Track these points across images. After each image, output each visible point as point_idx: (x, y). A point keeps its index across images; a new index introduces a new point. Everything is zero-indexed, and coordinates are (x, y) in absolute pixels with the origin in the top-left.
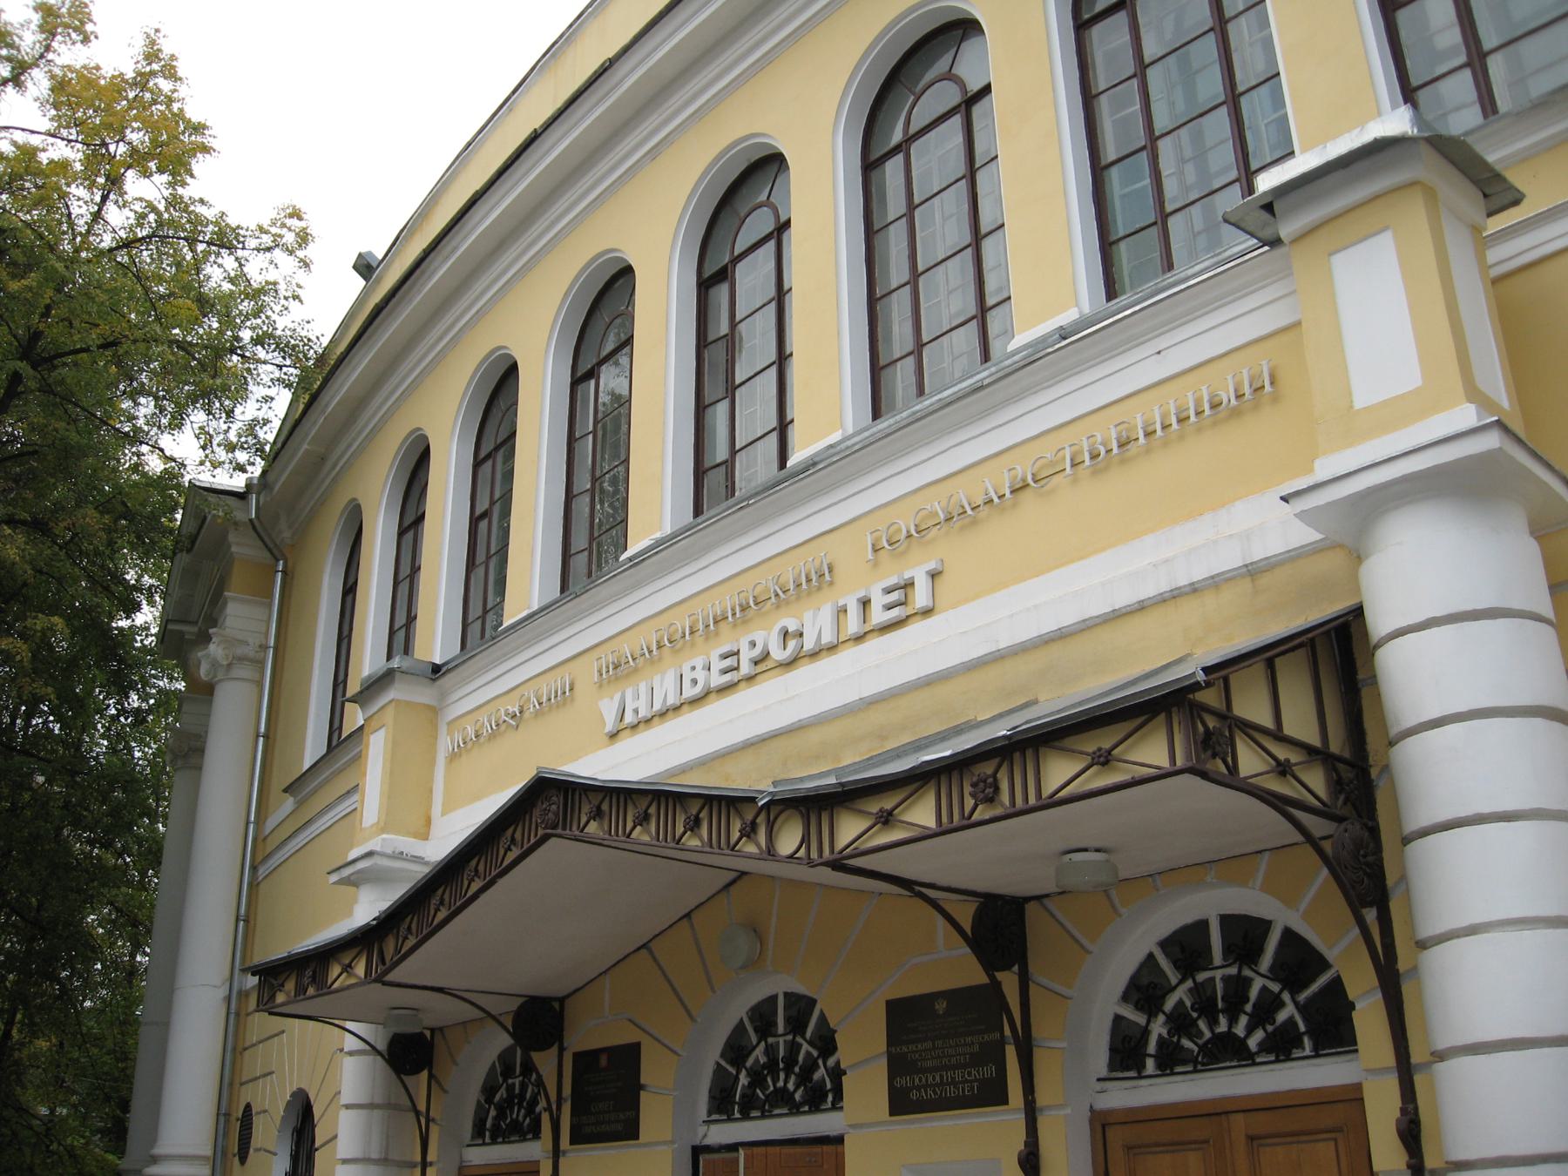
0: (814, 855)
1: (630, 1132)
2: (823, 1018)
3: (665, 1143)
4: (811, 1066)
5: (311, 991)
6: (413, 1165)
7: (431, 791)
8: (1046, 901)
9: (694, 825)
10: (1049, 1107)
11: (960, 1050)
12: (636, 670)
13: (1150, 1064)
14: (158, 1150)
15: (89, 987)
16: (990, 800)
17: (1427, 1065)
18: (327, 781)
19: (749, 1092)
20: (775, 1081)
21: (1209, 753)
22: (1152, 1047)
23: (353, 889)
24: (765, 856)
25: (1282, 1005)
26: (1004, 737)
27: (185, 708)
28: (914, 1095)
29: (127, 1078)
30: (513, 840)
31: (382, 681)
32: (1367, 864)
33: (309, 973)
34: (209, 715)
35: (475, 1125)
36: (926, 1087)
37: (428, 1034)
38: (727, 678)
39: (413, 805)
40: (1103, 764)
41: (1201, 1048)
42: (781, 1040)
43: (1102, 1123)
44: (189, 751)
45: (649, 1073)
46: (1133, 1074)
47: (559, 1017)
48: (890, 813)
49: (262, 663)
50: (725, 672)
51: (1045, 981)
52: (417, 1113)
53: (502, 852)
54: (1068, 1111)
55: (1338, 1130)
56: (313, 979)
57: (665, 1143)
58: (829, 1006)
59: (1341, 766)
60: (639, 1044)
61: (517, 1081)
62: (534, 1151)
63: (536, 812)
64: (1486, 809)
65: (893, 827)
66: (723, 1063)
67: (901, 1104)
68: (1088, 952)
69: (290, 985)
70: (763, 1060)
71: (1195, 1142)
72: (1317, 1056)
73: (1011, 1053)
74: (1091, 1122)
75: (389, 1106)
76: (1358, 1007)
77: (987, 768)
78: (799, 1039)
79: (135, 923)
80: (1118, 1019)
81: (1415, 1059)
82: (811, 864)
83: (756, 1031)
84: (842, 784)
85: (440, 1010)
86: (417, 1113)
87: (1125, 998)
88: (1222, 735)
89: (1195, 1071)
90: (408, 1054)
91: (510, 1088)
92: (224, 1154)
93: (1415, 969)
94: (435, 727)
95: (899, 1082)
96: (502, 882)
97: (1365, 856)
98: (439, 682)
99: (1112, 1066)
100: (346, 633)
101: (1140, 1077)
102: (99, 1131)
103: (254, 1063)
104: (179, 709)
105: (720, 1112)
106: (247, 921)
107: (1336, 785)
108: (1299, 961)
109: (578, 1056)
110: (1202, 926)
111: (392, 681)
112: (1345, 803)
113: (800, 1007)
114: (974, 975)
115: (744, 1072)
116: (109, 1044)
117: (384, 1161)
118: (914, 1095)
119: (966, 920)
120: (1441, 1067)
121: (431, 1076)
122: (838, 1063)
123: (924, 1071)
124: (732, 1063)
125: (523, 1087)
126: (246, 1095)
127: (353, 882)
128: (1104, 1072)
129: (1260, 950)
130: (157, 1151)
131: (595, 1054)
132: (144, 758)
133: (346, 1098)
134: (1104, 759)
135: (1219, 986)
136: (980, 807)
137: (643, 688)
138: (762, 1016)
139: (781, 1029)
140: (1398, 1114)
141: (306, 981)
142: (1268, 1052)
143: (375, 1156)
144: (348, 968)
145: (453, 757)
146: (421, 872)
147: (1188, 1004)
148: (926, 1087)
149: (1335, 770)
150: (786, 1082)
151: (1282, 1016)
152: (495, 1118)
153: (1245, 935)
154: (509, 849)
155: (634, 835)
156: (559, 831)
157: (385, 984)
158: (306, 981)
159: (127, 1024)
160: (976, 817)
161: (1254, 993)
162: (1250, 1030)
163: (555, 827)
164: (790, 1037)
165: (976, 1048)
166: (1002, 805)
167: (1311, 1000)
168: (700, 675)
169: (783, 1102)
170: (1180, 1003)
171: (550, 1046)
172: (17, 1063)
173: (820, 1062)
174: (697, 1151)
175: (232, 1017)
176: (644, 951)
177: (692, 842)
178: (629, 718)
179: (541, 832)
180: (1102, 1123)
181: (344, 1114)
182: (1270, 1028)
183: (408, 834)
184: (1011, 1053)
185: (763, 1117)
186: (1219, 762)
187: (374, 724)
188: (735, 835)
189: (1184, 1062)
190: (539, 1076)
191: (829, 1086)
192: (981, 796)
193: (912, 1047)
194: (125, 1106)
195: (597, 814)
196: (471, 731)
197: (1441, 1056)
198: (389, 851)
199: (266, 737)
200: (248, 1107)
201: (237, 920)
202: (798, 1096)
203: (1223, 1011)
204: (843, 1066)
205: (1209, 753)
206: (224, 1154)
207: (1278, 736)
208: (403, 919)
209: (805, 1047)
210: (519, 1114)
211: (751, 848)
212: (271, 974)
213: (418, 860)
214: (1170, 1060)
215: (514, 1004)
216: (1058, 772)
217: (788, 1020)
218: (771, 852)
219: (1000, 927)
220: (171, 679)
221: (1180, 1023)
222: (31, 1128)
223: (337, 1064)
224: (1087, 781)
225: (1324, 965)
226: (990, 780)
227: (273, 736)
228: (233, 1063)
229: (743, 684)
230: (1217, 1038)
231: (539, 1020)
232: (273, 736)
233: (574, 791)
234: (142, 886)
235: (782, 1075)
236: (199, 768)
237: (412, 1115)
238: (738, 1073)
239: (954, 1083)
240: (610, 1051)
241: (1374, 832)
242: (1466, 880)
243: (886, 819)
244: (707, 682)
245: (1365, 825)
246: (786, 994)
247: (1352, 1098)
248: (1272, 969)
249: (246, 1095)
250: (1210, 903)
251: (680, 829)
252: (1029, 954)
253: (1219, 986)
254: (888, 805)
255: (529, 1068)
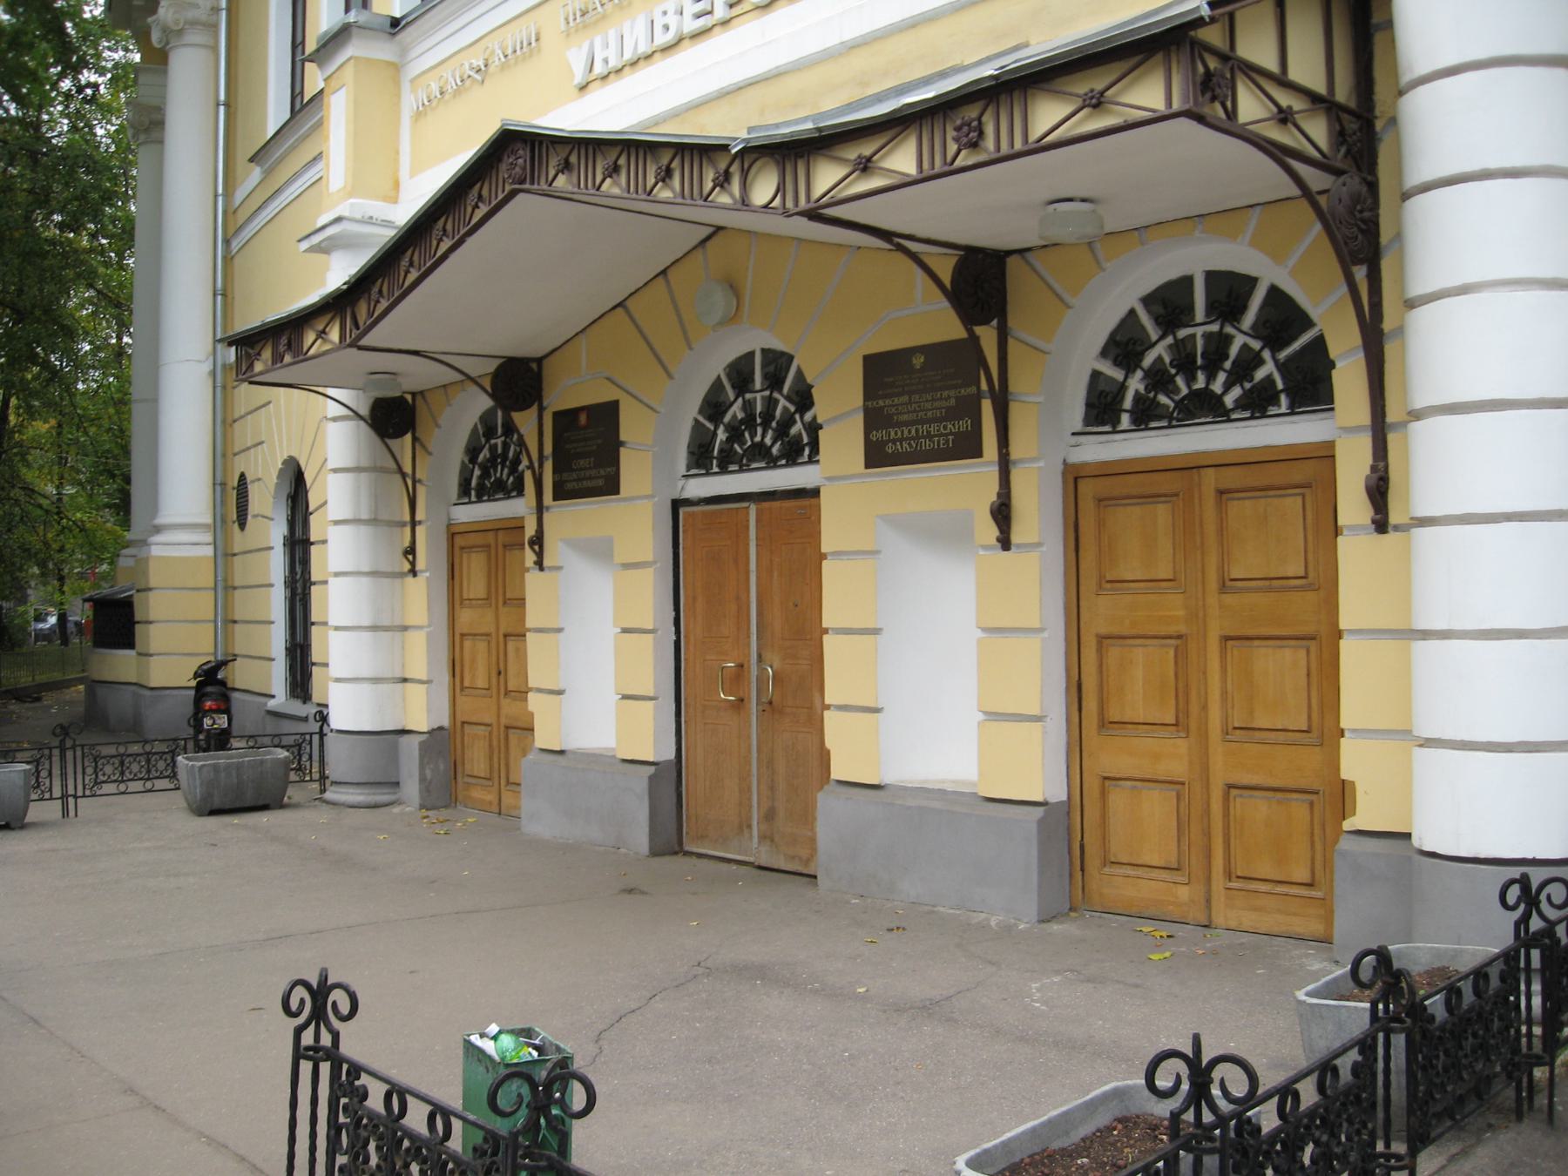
0: (790, 204)
1: (611, 487)
2: (800, 374)
3: (647, 497)
4: (788, 422)
5: (288, 359)
6: (403, 524)
7: (397, 153)
8: (1028, 255)
9: (666, 175)
10: (1022, 461)
11: (937, 404)
12: (604, 17)
13: (1125, 420)
14: (161, 520)
15: (79, 364)
16: (974, 145)
17: (1404, 424)
18: (293, 148)
19: (726, 447)
20: (752, 436)
21: (1208, 95)
22: (1128, 403)
23: (323, 257)
24: (739, 206)
25: (1261, 362)
26: (991, 77)
27: (142, 80)
28: (890, 449)
29: (126, 451)
30: (480, 197)
31: (340, 36)
32: (1363, 221)
33: (284, 340)
34: (164, 86)
35: (460, 485)
36: (901, 440)
37: (409, 397)
38: (701, 23)
39: (374, 168)
40: (1095, 106)
41: (1178, 404)
42: (758, 396)
43: (1074, 476)
44: (149, 125)
45: (629, 428)
46: (1107, 428)
47: (538, 377)
48: (869, 159)
49: (214, 27)
50: (698, 16)
51: (1023, 335)
52: (404, 475)
53: (469, 210)
54: (1041, 464)
55: (1308, 486)
56: (289, 345)
57: (647, 497)
58: (807, 362)
59: (1345, 117)
60: (617, 402)
61: (499, 441)
62: (519, 507)
63: (503, 167)
64: (1493, 164)
65: (872, 174)
66: (701, 419)
67: (876, 456)
68: (1069, 307)
69: (267, 354)
70: (740, 415)
71: (1165, 495)
72: (1292, 413)
73: (987, 407)
74: (1064, 474)
75: (375, 469)
76: (1339, 365)
77: (971, 112)
78: (776, 395)
79: (118, 305)
80: (1096, 375)
81: (1390, 419)
82: (787, 214)
83: (733, 387)
84: (819, 129)
85: (415, 375)
86: (404, 475)
87: (1104, 353)
88: (1223, 76)
89: (1170, 427)
90: (391, 418)
91: (493, 448)
92: (224, 521)
93: (1400, 331)
94: (397, 83)
95: (875, 436)
96: (470, 241)
97: (1361, 212)
98: (399, 37)
99: (1088, 421)
100: (299, 39)
101: (1115, 432)
102: (108, 506)
103: (244, 434)
104: (135, 81)
105: (698, 466)
106: (224, 295)
107: (1339, 136)
108: (1284, 319)
109: (558, 416)
110: (1186, 282)
111: (349, 37)
112: (1345, 156)
113: (777, 364)
114: (949, 327)
115: (721, 428)
116: (106, 423)
117: (374, 521)
118: (890, 449)
119: (945, 271)
120: (1416, 427)
121: (415, 439)
122: (815, 418)
123: (900, 424)
124: (710, 419)
125: (506, 446)
126: (240, 465)
127: (323, 249)
128: (1079, 427)
129: (1243, 308)
130: (160, 521)
131: (574, 412)
132: (108, 135)
133: (331, 465)
134: (1097, 103)
135: (1200, 343)
136: (963, 153)
137: (612, 35)
138: (740, 373)
139: (758, 385)
140: (1368, 471)
141: (282, 348)
142: (1244, 409)
143: (365, 516)
144: (322, 334)
145: (419, 115)
146: (389, 234)
147: (1167, 360)
148: (901, 440)
149: (1339, 120)
150: (763, 436)
151: (1260, 374)
152: (480, 477)
153: (1229, 292)
154: (476, 206)
155: (605, 187)
156: (527, 186)
157: (360, 348)
158: (282, 348)
159: (122, 402)
160: (959, 163)
161: (1234, 350)
162: (1228, 387)
163: (522, 182)
164: (767, 393)
165: (953, 402)
166: (986, 150)
167: (1289, 359)
168: (672, 20)
169: (761, 456)
170: (1160, 358)
171: (529, 407)
172: (20, 444)
173: (797, 417)
174: (677, 504)
175: (219, 390)
176: (620, 310)
177: (664, 194)
178: (599, 69)
179: (508, 188)
180: (1074, 476)
181: (332, 477)
182: (1248, 385)
183: (377, 198)
184: (987, 407)
185: (741, 471)
186: (1217, 106)
187: (333, 83)
188: (709, 185)
189: (1159, 418)
190: (521, 437)
191: (806, 440)
192: (965, 140)
193: (888, 402)
194: (127, 480)
195: (566, 167)
196: (435, 88)
197: (1417, 415)
198: (358, 216)
199: (227, 105)
200: (242, 476)
201: (215, 295)
202: (775, 450)
203: (1200, 368)
204: (819, 421)
205: (1208, 95)
206: (224, 521)
207: (1283, 82)
208: (374, 283)
209: (783, 402)
210: (502, 473)
211: (724, 199)
212: (249, 343)
213: (387, 224)
214: (1145, 416)
215: (492, 366)
216: (1047, 115)
217: (765, 376)
218: (745, 202)
219: (981, 282)
220: (126, 50)
221: (1159, 379)
222: (40, 506)
223: (319, 427)
224: (1070, 129)
225: (1306, 322)
226: (975, 124)
227: (234, 104)
228: (225, 435)
229: (717, 29)
230: (1194, 394)
231: (517, 381)
232: (234, 104)
233: (541, 143)
234: (122, 267)
235: (759, 430)
236: (161, 142)
237: (398, 477)
238: (716, 428)
239: (929, 436)
240: (588, 409)
241: (1373, 187)
242: (1454, 237)
243: (865, 166)
244: (680, 27)
245: (1364, 179)
246: (763, 351)
247: (1324, 455)
248: (1254, 326)
249: (240, 465)
250: (1196, 258)
251: (651, 180)
252: (1010, 308)
253: (1200, 343)
254: (867, 152)
255: (510, 428)
